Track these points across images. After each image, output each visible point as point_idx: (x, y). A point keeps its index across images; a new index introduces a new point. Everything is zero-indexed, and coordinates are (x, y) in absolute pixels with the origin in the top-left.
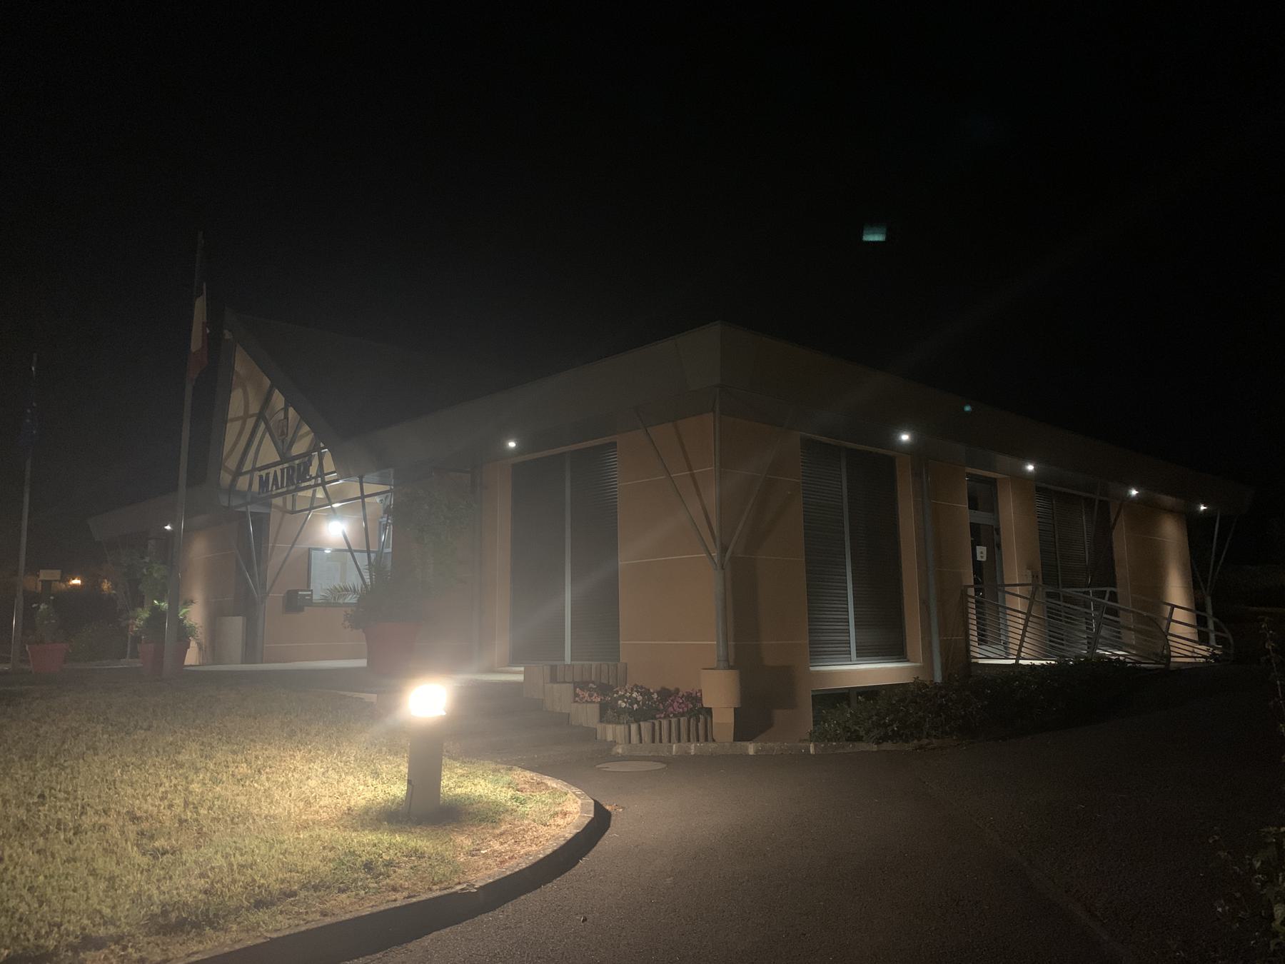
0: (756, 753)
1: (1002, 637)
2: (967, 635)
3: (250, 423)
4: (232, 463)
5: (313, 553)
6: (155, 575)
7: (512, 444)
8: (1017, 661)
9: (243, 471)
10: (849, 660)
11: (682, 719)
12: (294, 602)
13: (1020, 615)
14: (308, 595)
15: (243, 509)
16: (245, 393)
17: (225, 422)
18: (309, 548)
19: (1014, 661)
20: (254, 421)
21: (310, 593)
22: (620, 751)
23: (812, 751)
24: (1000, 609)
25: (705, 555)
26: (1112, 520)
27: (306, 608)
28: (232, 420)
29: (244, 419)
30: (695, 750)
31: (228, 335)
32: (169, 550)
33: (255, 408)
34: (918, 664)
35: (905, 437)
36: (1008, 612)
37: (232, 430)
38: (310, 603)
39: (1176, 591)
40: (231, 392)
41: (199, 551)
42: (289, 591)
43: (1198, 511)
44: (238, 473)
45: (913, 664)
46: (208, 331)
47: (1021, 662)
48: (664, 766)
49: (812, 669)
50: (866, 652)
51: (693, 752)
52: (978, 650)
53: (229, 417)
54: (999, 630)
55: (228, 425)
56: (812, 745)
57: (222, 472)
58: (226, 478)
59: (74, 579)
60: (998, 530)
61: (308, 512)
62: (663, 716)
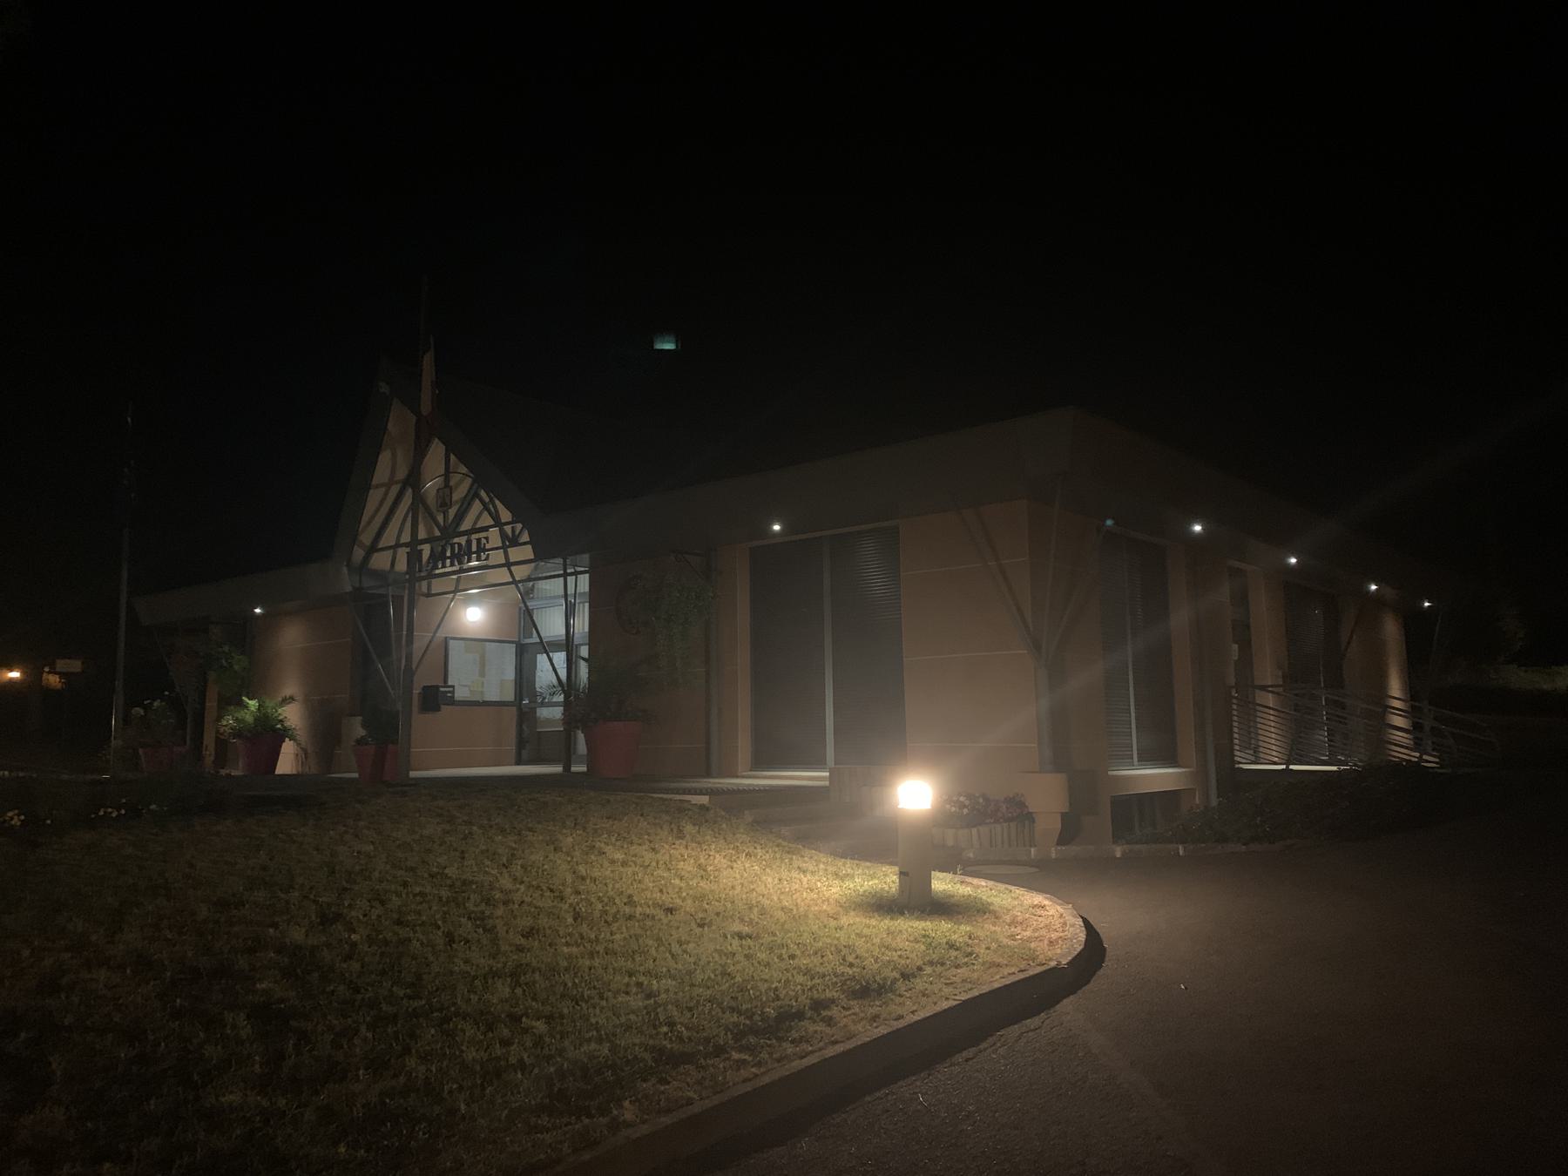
0: (1123, 855)
1: (1253, 741)
2: (1231, 739)
3: (395, 489)
4: (366, 538)
5: (452, 643)
6: (236, 667)
7: (777, 527)
8: (1287, 767)
9: (380, 547)
10: (1131, 765)
11: (1011, 824)
12: (435, 698)
13: (1272, 712)
14: (449, 692)
15: (381, 591)
16: (394, 455)
17: (366, 487)
18: (446, 638)
19: (1284, 767)
20: (399, 489)
21: (451, 689)
22: (971, 855)
23: (1181, 853)
24: (1251, 706)
25: (1026, 652)
26: (363, 523)
27: (442, 706)
28: (377, 487)
29: (388, 486)
30: (1056, 854)
31: (384, 388)
32: (245, 635)
33: (402, 474)
34: (1192, 769)
35: (1198, 528)
36: (1258, 708)
37: (374, 497)
38: (452, 702)
39: (1395, 687)
40: (378, 453)
41: (292, 638)
42: (424, 687)
43: (1423, 607)
44: (373, 549)
45: (1184, 770)
46: (437, 392)
47: (1291, 767)
48: (1037, 870)
49: (1110, 773)
50: (1148, 758)
51: (1053, 856)
52: (1242, 755)
53: (374, 483)
54: (1250, 727)
55: (371, 491)
56: (1180, 847)
57: (356, 546)
58: (358, 553)
59: (11, 671)
60: (1248, 626)
61: (451, 596)
62: (992, 821)
